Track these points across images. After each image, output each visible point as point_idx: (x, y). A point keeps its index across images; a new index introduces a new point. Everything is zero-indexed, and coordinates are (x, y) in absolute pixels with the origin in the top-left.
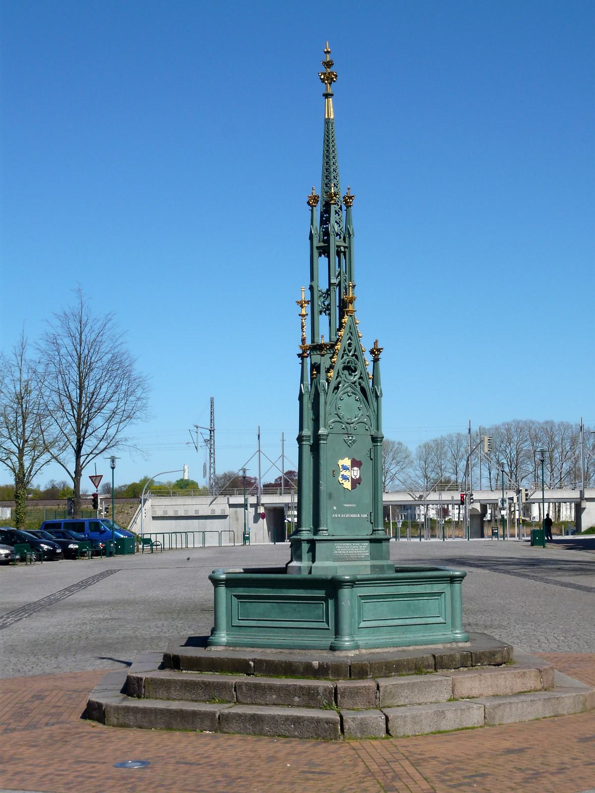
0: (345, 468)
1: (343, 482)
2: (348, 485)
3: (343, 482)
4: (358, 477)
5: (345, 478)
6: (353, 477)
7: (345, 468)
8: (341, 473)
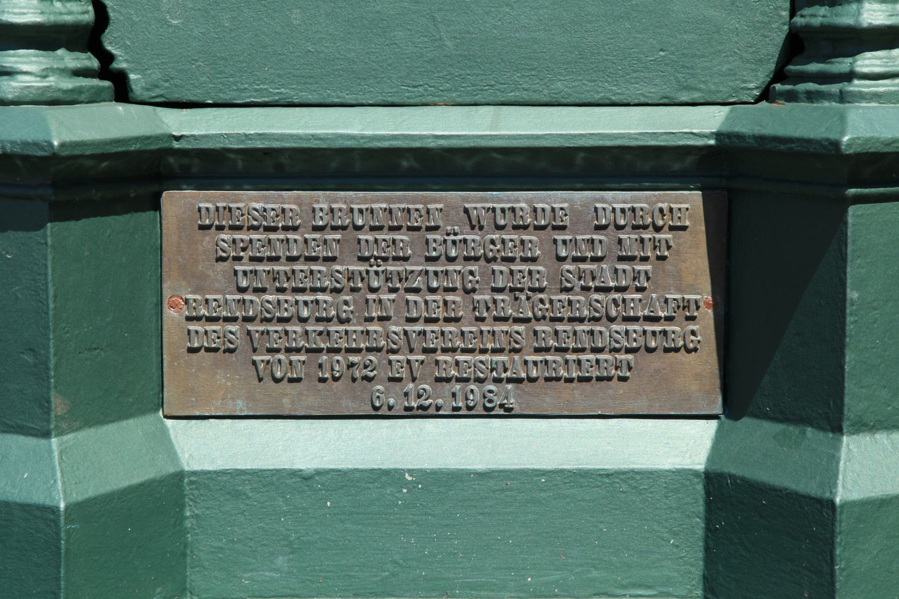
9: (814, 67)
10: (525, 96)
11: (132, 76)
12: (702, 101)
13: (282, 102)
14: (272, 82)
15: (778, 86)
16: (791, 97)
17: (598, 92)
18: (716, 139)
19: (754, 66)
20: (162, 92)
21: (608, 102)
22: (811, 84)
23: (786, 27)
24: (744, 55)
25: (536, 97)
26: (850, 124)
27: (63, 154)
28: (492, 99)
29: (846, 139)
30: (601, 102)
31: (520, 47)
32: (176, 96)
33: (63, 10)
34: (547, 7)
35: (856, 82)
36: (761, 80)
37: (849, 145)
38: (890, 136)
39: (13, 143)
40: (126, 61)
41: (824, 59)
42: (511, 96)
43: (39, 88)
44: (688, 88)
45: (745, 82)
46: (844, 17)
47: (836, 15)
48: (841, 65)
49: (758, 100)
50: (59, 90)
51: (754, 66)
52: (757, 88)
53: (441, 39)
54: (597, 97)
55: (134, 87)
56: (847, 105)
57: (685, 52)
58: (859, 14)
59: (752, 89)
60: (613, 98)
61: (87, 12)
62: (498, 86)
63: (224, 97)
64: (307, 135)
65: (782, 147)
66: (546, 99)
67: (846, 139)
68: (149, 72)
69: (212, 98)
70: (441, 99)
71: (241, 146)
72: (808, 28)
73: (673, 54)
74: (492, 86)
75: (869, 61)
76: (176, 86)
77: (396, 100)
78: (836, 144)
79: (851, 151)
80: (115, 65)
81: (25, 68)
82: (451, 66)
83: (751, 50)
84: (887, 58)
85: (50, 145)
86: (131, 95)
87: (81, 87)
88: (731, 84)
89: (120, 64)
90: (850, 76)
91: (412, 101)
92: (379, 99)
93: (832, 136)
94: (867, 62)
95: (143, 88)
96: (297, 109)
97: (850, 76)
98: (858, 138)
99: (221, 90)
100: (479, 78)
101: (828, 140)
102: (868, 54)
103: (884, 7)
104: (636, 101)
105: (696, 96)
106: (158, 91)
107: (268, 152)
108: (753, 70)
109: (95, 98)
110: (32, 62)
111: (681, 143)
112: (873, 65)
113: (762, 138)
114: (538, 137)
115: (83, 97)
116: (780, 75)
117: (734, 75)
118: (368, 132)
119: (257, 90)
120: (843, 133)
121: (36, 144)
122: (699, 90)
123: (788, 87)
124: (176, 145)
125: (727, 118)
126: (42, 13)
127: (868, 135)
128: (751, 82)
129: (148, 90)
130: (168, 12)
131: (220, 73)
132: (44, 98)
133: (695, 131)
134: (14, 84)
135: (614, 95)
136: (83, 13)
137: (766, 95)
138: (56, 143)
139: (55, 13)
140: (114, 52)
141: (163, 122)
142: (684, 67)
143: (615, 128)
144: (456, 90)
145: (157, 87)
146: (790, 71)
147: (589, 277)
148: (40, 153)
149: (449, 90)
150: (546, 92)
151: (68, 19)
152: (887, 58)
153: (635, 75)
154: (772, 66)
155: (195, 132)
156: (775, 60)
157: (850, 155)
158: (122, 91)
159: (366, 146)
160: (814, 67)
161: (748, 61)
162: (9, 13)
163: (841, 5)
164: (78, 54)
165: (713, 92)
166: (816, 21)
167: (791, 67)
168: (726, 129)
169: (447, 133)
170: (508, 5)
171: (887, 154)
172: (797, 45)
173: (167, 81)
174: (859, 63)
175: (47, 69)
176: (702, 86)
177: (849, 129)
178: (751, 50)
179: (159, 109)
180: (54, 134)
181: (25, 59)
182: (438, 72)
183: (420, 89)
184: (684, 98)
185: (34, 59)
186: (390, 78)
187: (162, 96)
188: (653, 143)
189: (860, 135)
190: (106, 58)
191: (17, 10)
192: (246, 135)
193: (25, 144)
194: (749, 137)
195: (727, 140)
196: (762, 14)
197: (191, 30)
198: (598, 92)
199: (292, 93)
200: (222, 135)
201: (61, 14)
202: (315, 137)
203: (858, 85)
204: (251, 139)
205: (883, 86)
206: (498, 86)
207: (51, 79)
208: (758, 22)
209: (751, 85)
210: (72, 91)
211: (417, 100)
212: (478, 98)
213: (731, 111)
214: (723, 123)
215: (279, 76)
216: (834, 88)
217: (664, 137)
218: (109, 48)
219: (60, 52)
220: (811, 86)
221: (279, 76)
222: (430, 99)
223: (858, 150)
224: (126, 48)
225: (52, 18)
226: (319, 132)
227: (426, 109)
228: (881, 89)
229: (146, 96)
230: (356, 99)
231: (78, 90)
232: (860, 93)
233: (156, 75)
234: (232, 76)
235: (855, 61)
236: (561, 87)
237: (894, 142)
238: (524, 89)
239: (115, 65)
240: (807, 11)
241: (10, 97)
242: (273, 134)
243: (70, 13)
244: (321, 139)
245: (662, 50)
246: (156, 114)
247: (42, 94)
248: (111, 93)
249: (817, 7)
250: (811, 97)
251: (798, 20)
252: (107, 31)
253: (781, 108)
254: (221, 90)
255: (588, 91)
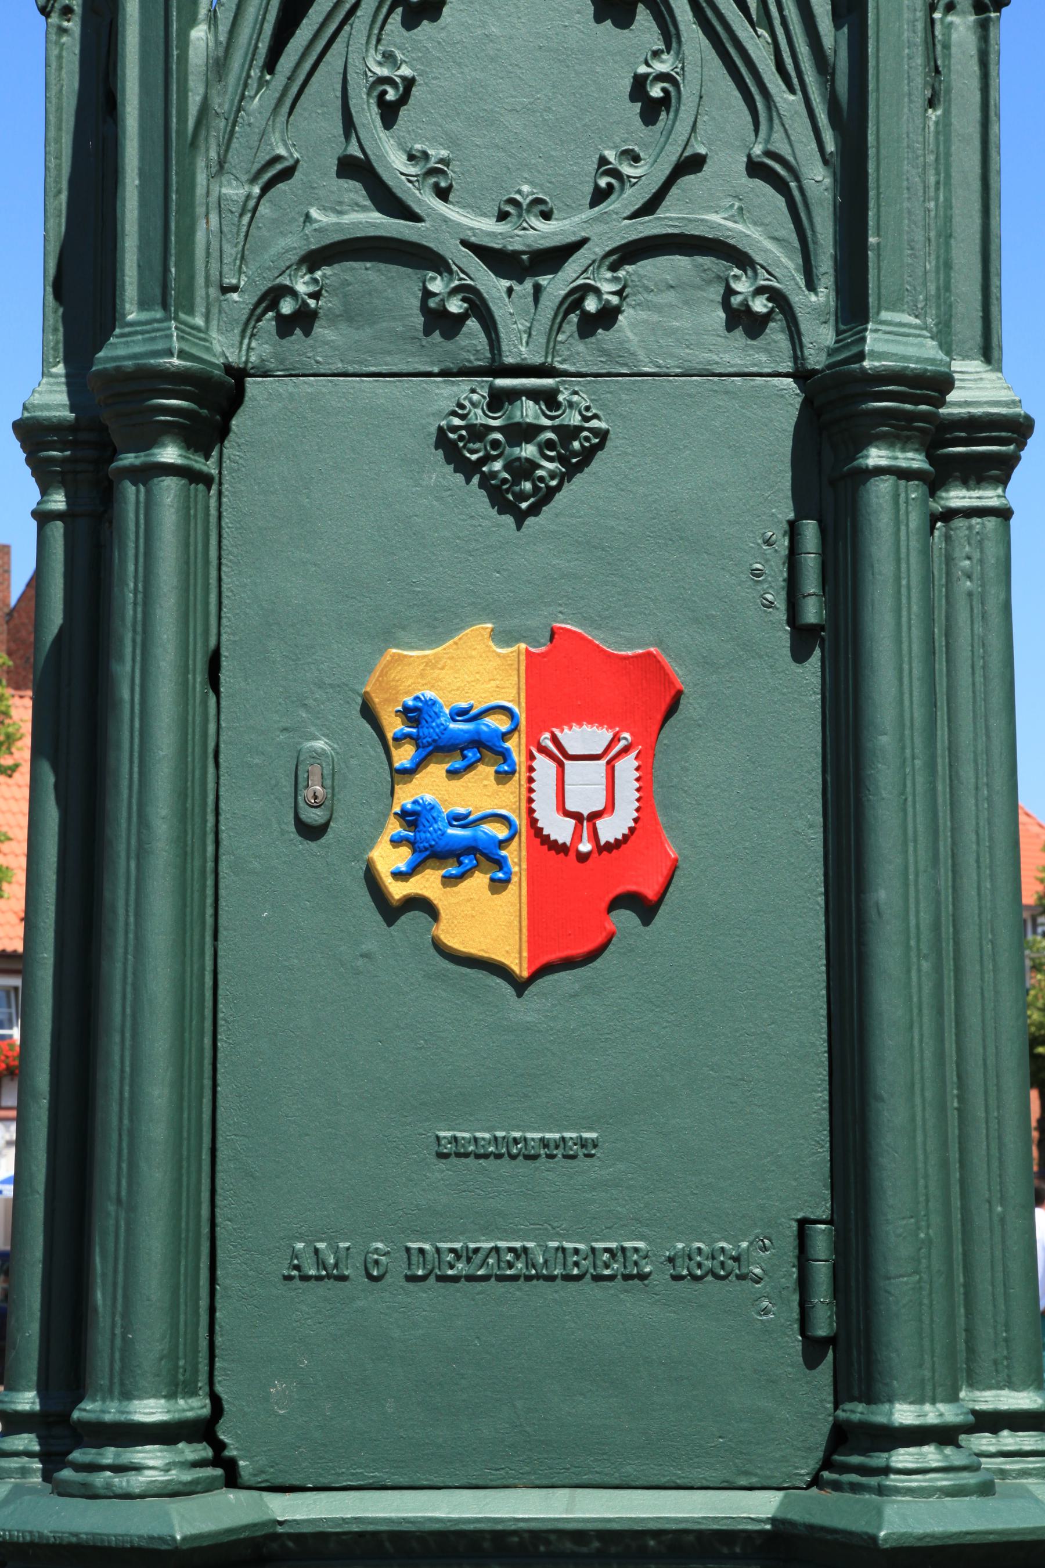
0: (469, 746)
1: (427, 884)
2: (485, 919)
3: (427, 884)
4: (610, 830)
5: (461, 853)
6: (560, 830)
7: (469, 746)
8: (405, 796)
9: (855, 1459)
10: (598, 1479)
11: (241, 1463)
12: (759, 1485)
13: (376, 1485)
14: (368, 1466)
15: (826, 1474)
16: (837, 1486)
17: (664, 1476)
18: (772, 1524)
19: (804, 1454)
20: (268, 1477)
21: (673, 1485)
22: (854, 1475)
23: (831, 1418)
24: (795, 1443)
25: (607, 1480)
26: (886, 1518)
27: (184, 1547)
28: (566, 1482)
29: (882, 1534)
30: (667, 1485)
31: (593, 1433)
32: (279, 1481)
33: (186, 1407)
34: (616, 1396)
35: (892, 1476)
36: (812, 1467)
37: (886, 1539)
38: (921, 1531)
39: (140, 1537)
40: (237, 1449)
41: (864, 1452)
42: (585, 1479)
43: (162, 1482)
44: (747, 1473)
45: (797, 1468)
46: (878, 1415)
47: (872, 1413)
48: (878, 1459)
49: (809, 1486)
50: (180, 1483)
51: (804, 1454)
52: (808, 1474)
53: (521, 1425)
54: (663, 1480)
55: (242, 1473)
56: (885, 1498)
57: (742, 1439)
58: (891, 1414)
59: (803, 1475)
60: (678, 1481)
61: (204, 1406)
62: (573, 1470)
63: (324, 1481)
64: (399, 1518)
65: (829, 1537)
66: (617, 1482)
67: (882, 1534)
68: (256, 1459)
69: (312, 1483)
70: (521, 1482)
71: (338, 1530)
72: (848, 1422)
73: (730, 1440)
74: (568, 1469)
75: (903, 1457)
76: (281, 1471)
77: (481, 1483)
78: (874, 1538)
79: (888, 1546)
80: (227, 1453)
81: (151, 1463)
82: (530, 1450)
83: (801, 1439)
84: (917, 1454)
85: (174, 1539)
86: (239, 1480)
87: (198, 1478)
88: (784, 1470)
89: (231, 1452)
90: (887, 1470)
91: (494, 1483)
92: (464, 1481)
93: (870, 1530)
94: (901, 1458)
95: (251, 1474)
96: (390, 1492)
97: (887, 1470)
98: (893, 1534)
99: (321, 1475)
100: (557, 1462)
101: (867, 1534)
102: (902, 1451)
103: (912, 1408)
104: (699, 1485)
105: (754, 1480)
106: (264, 1477)
107: (361, 1535)
108: (804, 1458)
109: (208, 1487)
110: (157, 1457)
111: (740, 1527)
112: (906, 1461)
113: (811, 1527)
114: (609, 1520)
115: (199, 1488)
116: (827, 1464)
117: (787, 1461)
118: (455, 1515)
119: (353, 1474)
120: (880, 1529)
121: (161, 1539)
122: (756, 1475)
123: (835, 1476)
124: (280, 1530)
125: (782, 1504)
126: (168, 1412)
127: (903, 1530)
128: (802, 1468)
129: (255, 1475)
130: (276, 1403)
131: (320, 1458)
132: (166, 1491)
133: (752, 1516)
134: (141, 1479)
135: (679, 1478)
136: (202, 1407)
137: (816, 1481)
138: (178, 1537)
139: (178, 1411)
140: (226, 1441)
141: (268, 1507)
142: (741, 1453)
143: (679, 1513)
144: (535, 1473)
145: (263, 1472)
146: (836, 1461)
147: (590, 1146)
148: (164, 1547)
149: (528, 1473)
150: (617, 1475)
151: (190, 1414)
152: (917, 1454)
153: (697, 1460)
154: (820, 1454)
155: (298, 1517)
156: (823, 1448)
157: (887, 1549)
158: (232, 1479)
159: (452, 1529)
160: (855, 1459)
161: (799, 1450)
162: (140, 1413)
163: (875, 1404)
164: (195, 1445)
165: (769, 1478)
166: (856, 1417)
167: (836, 1457)
168: (780, 1515)
169: (526, 1516)
170: (581, 1394)
171: (919, 1548)
172: (842, 1437)
173: (272, 1467)
174: (893, 1459)
175: (169, 1463)
176: (758, 1471)
177: (886, 1525)
178: (801, 1439)
179: (265, 1494)
180: (177, 1528)
181: (151, 1455)
182: (519, 1456)
183: (502, 1472)
184: (743, 1482)
185: (159, 1454)
186: (474, 1462)
187: (267, 1481)
188: (715, 1527)
189: (895, 1530)
190: (219, 1446)
191: (148, 1410)
192: (343, 1519)
193: (151, 1538)
194: (800, 1524)
195: (781, 1526)
196: (809, 1405)
197: (296, 1419)
198: (664, 1476)
199: (386, 1476)
200: (321, 1519)
201: (184, 1410)
202: (406, 1520)
203: (894, 1480)
204: (347, 1523)
205: (915, 1482)
206: (573, 1470)
207: (173, 1472)
208: (806, 1413)
209: (803, 1472)
210: (191, 1483)
211: (498, 1483)
212: (554, 1481)
213: (785, 1497)
214: (778, 1509)
215: (374, 1460)
216: (873, 1481)
217: (725, 1521)
218: (222, 1437)
219: (181, 1445)
220: (854, 1478)
221: (374, 1460)
222: (511, 1481)
223: (894, 1544)
224: (237, 1437)
225: (177, 1416)
226: (410, 1515)
227: (507, 1491)
228: (914, 1484)
229: (252, 1481)
230: (443, 1482)
231: (195, 1482)
232: (896, 1487)
233: (262, 1461)
234: (330, 1461)
235: (890, 1457)
236: (630, 1470)
237: (925, 1537)
238: (597, 1472)
239: (227, 1453)
240: (848, 1406)
241: (137, 1491)
242: (368, 1518)
243: (191, 1409)
244: (411, 1522)
245: (720, 1437)
246: (262, 1500)
247: (165, 1487)
248: (222, 1481)
249: (856, 1403)
250: (855, 1488)
251: (839, 1413)
252: (221, 1421)
253: (829, 1496)
254: (321, 1475)
255: (655, 1475)
